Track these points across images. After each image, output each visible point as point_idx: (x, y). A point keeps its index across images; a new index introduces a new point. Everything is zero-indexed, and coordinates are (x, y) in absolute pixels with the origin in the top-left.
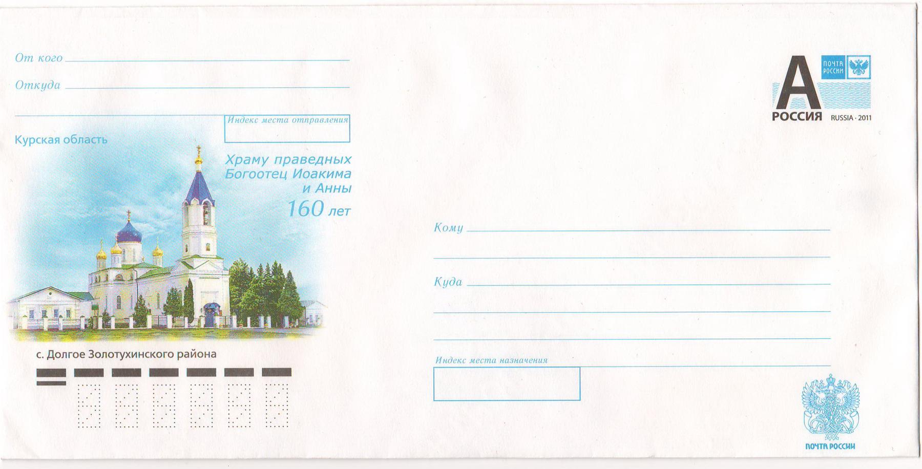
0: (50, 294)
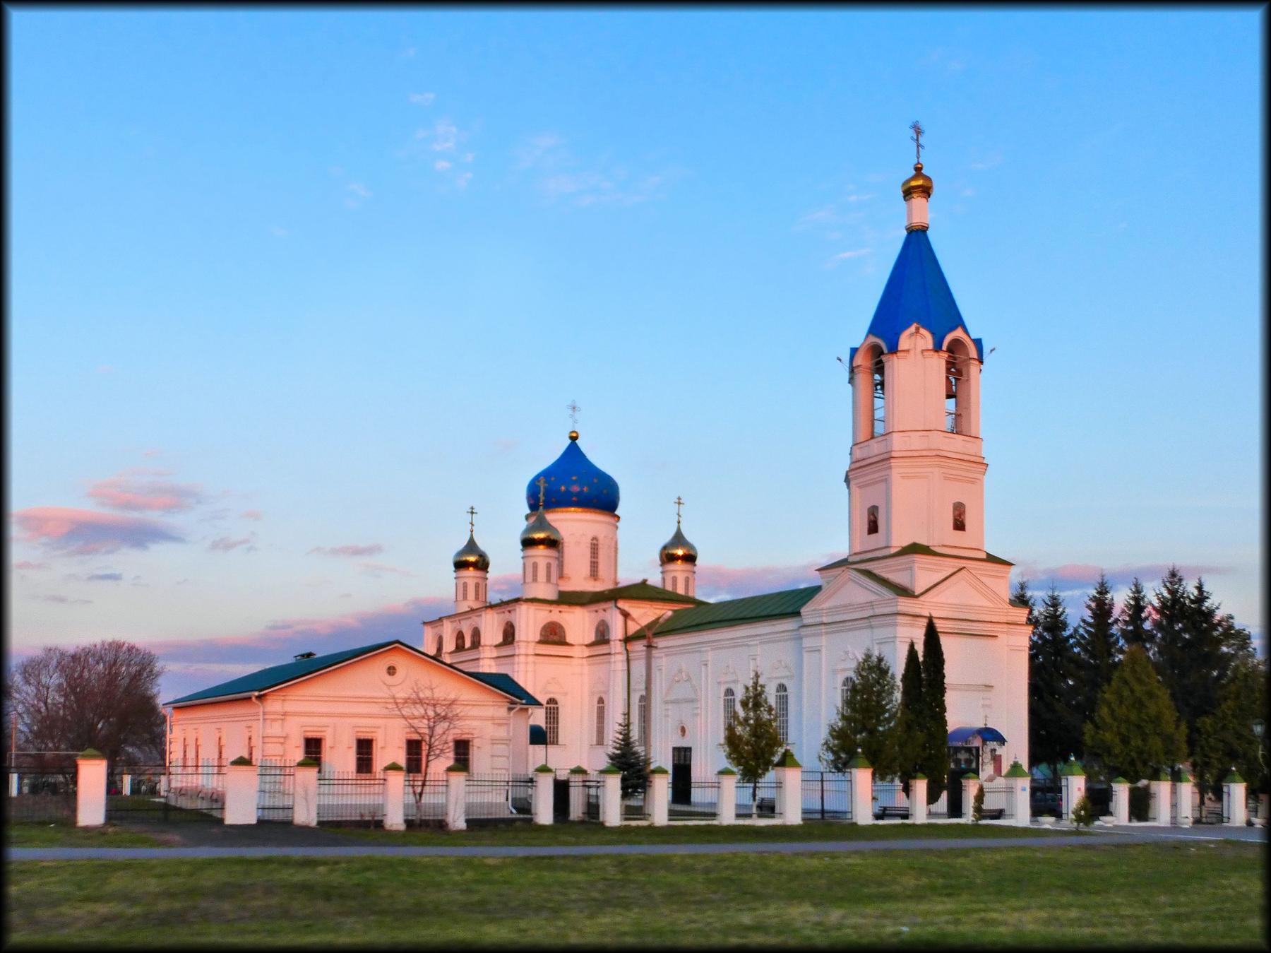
0: (391, 671)
